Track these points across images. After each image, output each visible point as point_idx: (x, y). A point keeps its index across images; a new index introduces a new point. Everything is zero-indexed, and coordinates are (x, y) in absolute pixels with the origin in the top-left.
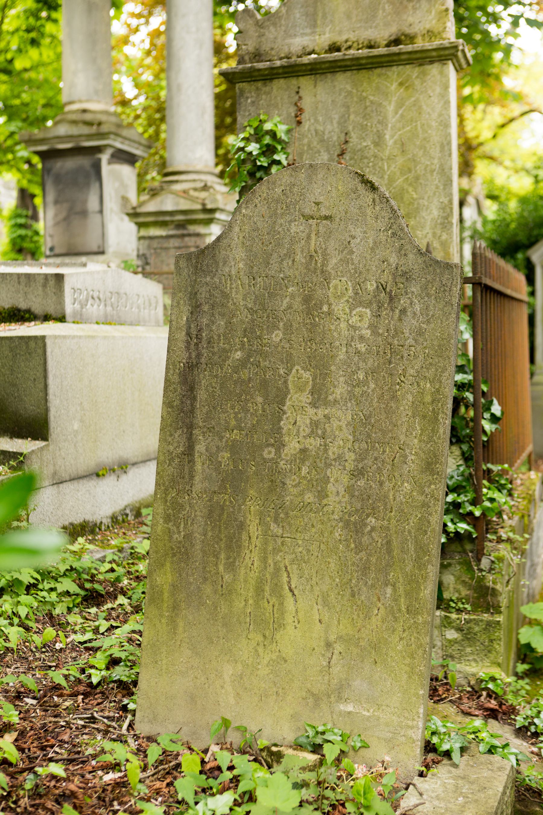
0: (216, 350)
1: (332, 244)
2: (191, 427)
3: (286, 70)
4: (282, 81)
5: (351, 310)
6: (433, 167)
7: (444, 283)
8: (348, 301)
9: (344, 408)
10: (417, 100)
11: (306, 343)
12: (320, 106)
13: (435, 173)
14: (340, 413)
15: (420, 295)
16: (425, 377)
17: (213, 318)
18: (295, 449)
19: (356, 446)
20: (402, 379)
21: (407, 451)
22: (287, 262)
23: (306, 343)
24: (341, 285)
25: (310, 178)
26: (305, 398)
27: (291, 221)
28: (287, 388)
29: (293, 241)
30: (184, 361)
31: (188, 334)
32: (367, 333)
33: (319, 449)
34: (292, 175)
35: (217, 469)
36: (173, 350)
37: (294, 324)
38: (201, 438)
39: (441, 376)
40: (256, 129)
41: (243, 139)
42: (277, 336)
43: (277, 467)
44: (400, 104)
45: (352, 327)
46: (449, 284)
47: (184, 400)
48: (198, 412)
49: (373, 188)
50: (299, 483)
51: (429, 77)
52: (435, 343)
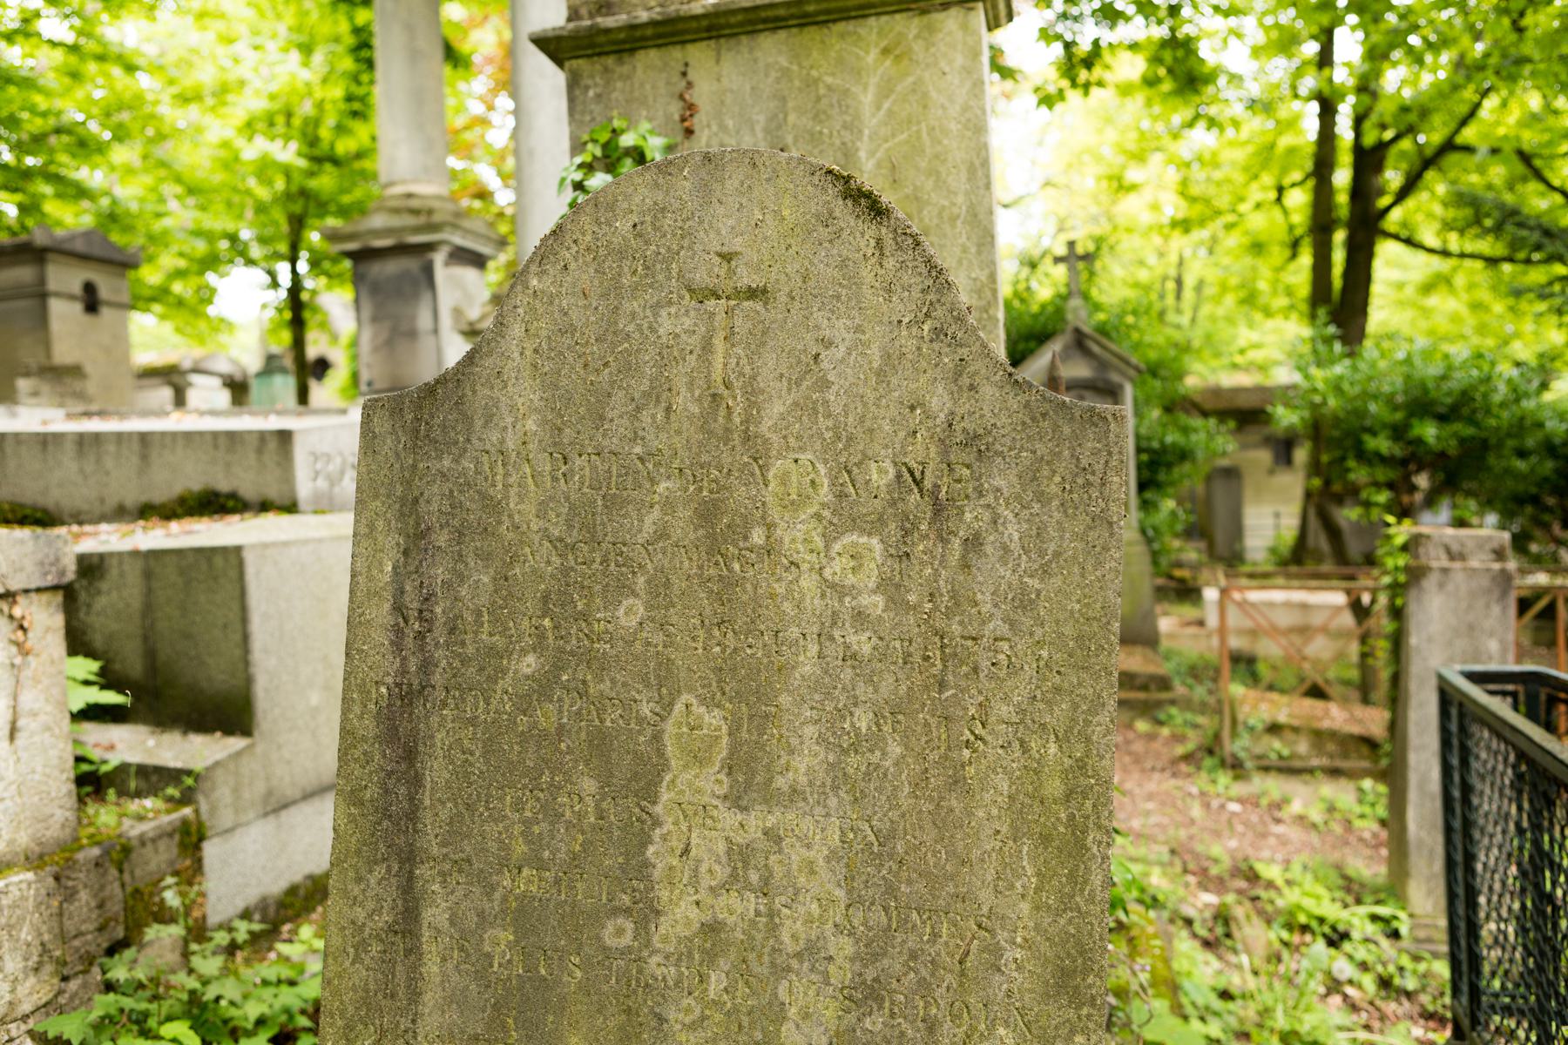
0: (470, 650)
1: (770, 365)
2: (409, 858)
3: (661, 30)
4: (653, 53)
5: (828, 542)
6: (956, 210)
7: (1084, 462)
8: (818, 516)
9: (818, 810)
10: (919, 82)
11: (709, 631)
12: (729, 99)
13: (959, 223)
14: (807, 824)
15: (1018, 498)
16: (1043, 726)
17: (460, 566)
18: (688, 923)
19: (858, 918)
20: (979, 730)
21: (1002, 936)
22: (652, 415)
23: (709, 631)
24: (798, 472)
25: (704, 190)
26: (711, 782)
27: (657, 306)
28: (661, 753)
29: (666, 357)
30: (389, 680)
31: (398, 608)
32: (875, 603)
33: (753, 923)
34: (657, 185)
35: (481, 975)
36: (360, 651)
37: (673, 579)
38: (436, 887)
39: (1087, 723)
40: (605, 146)
41: (580, 166)
42: (630, 613)
43: (640, 971)
44: (886, 91)
45: (833, 586)
46: (1099, 467)
47: (391, 783)
48: (427, 817)
49: (876, 209)
50: (703, 1018)
51: (940, 36)
52: (1068, 630)
